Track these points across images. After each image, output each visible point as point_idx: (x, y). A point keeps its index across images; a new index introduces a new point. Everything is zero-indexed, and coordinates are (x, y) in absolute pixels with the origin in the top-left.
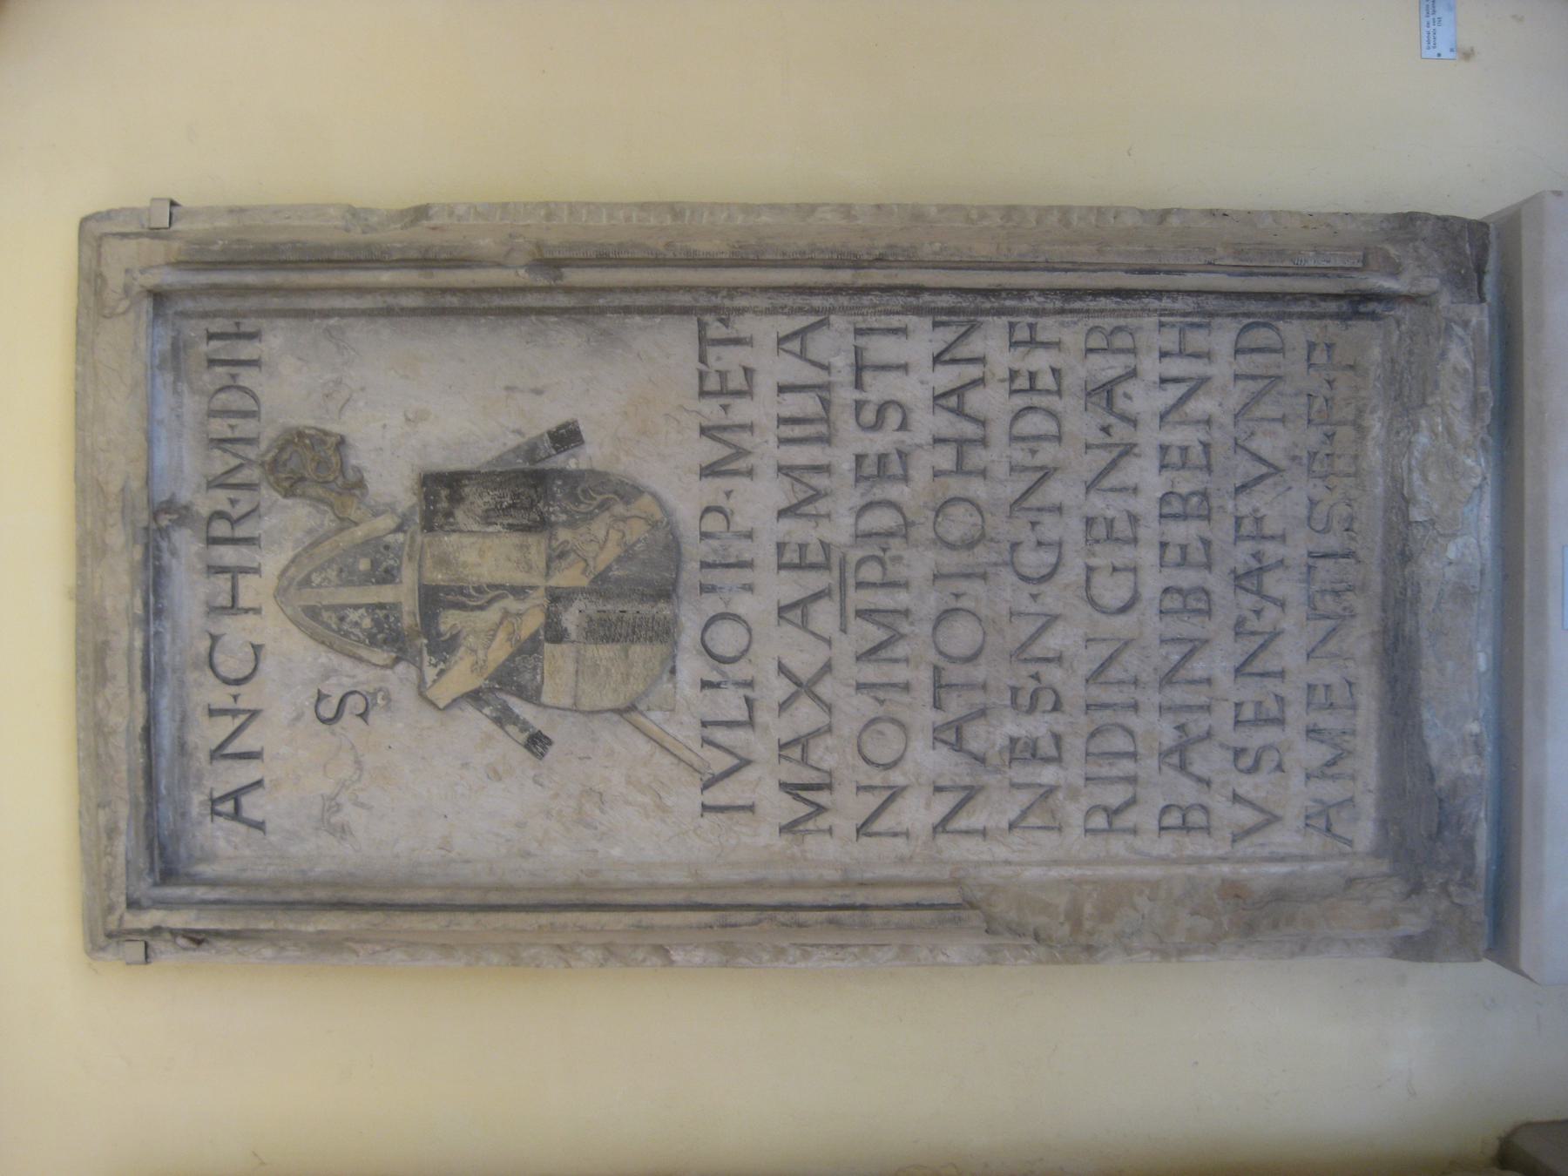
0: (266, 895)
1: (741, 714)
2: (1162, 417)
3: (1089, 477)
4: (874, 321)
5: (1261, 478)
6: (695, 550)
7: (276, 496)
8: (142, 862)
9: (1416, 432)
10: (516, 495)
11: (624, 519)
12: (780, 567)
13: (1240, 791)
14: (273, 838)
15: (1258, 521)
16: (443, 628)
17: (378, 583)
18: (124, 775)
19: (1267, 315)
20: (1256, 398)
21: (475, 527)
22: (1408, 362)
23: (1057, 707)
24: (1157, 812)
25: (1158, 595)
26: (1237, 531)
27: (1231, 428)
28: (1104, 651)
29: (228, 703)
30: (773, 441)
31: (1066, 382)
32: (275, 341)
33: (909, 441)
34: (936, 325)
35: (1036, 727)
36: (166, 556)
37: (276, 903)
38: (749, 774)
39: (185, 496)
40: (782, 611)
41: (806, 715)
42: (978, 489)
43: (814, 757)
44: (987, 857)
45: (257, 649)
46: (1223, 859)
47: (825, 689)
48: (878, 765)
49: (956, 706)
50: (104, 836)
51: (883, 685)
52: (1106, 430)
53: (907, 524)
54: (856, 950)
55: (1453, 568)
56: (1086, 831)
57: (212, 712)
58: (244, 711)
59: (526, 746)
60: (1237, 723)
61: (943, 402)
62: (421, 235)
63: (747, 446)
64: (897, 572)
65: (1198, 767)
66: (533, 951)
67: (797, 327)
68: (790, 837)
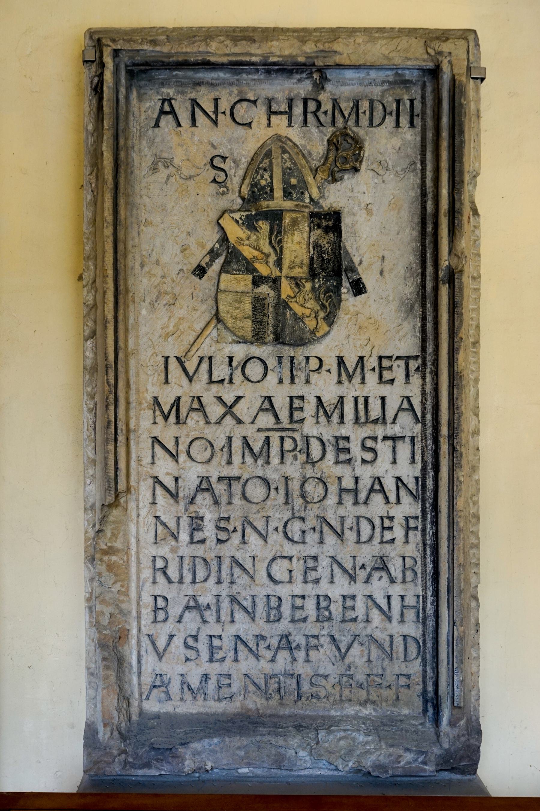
0: (122, 125)
1: (215, 378)
2: (370, 597)
3: (338, 558)
4: (418, 446)
5: (339, 649)
6: (300, 353)
7: (329, 135)
8: (138, 59)
9: (366, 734)
10: (329, 261)
11: (316, 317)
12: (291, 398)
13: (175, 638)
14: (150, 132)
15: (316, 647)
16: (260, 222)
17: (284, 188)
18: (184, 50)
19: (425, 653)
20: (380, 646)
21: (312, 240)
22: (402, 729)
23: (219, 541)
24: (164, 594)
25: (277, 594)
26: (311, 636)
27: (364, 633)
28: (248, 565)
29: (221, 109)
30: (356, 394)
31: (387, 546)
32: (409, 136)
33: (356, 464)
34: (417, 478)
35: (209, 531)
36: (298, 76)
37: (117, 130)
38: (185, 381)
39: (329, 87)
40: (269, 399)
41: (215, 411)
42: (332, 499)
43: (193, 415)
44: (141, 505)
45: (249, 125)
46: (139, 630)
47: (228, 420)
48: (189, 448)
49: (220, 488)
50: (152, 38)
51: (230, 450)
52: (363, 567)
53: (313, 463)
54: (93, 436)
55: (294, 754)
56: (155, 557)
57: (216, 100)
58: (217, 117)
59: (199, 265)
60: (211, 637)
61: (377, 482)
62: (467, 211)
63: (354, 381)
64: (289, 457)
65: (187, 615)
66: (92, 267)
67: (415, 407)
68: (152, 402)
